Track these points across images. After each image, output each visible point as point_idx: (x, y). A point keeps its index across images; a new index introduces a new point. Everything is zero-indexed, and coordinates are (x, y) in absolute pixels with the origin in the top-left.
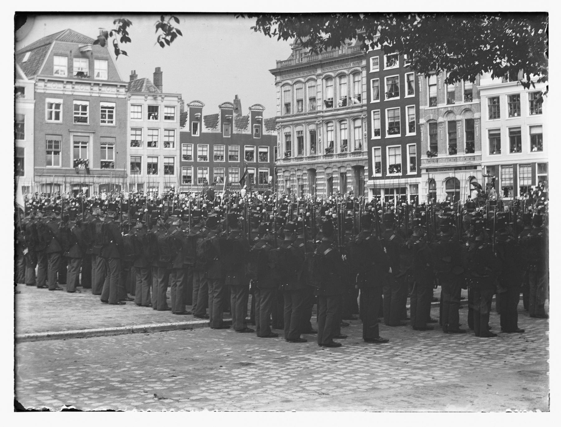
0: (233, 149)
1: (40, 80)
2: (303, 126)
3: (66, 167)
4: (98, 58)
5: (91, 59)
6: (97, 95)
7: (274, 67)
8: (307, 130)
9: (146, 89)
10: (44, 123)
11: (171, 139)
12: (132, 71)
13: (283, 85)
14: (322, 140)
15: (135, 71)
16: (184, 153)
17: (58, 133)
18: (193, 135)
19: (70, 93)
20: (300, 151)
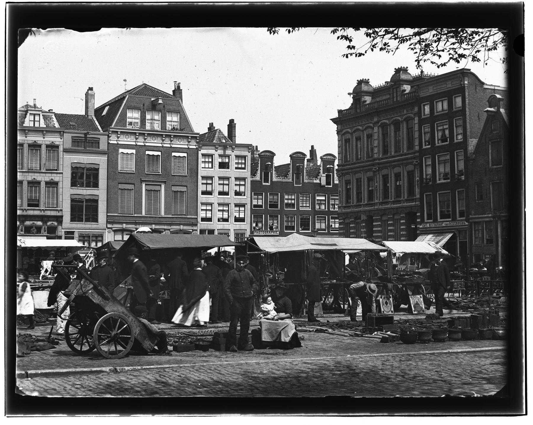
1: (113, 132)
4: (171, 112)
5: (163, 111)
6: (169, 146)
7: (336, 115)
8: (365, 177)
9: (218, 140)
11: (242, 189)
12: (210, 123)
13: (344, 134)
14: (378, 187)
15: (212, 123)
16: (255, 202)
17: (130, 181)
18: (264, 184)
19: (143, 144)
20: (359, 199)
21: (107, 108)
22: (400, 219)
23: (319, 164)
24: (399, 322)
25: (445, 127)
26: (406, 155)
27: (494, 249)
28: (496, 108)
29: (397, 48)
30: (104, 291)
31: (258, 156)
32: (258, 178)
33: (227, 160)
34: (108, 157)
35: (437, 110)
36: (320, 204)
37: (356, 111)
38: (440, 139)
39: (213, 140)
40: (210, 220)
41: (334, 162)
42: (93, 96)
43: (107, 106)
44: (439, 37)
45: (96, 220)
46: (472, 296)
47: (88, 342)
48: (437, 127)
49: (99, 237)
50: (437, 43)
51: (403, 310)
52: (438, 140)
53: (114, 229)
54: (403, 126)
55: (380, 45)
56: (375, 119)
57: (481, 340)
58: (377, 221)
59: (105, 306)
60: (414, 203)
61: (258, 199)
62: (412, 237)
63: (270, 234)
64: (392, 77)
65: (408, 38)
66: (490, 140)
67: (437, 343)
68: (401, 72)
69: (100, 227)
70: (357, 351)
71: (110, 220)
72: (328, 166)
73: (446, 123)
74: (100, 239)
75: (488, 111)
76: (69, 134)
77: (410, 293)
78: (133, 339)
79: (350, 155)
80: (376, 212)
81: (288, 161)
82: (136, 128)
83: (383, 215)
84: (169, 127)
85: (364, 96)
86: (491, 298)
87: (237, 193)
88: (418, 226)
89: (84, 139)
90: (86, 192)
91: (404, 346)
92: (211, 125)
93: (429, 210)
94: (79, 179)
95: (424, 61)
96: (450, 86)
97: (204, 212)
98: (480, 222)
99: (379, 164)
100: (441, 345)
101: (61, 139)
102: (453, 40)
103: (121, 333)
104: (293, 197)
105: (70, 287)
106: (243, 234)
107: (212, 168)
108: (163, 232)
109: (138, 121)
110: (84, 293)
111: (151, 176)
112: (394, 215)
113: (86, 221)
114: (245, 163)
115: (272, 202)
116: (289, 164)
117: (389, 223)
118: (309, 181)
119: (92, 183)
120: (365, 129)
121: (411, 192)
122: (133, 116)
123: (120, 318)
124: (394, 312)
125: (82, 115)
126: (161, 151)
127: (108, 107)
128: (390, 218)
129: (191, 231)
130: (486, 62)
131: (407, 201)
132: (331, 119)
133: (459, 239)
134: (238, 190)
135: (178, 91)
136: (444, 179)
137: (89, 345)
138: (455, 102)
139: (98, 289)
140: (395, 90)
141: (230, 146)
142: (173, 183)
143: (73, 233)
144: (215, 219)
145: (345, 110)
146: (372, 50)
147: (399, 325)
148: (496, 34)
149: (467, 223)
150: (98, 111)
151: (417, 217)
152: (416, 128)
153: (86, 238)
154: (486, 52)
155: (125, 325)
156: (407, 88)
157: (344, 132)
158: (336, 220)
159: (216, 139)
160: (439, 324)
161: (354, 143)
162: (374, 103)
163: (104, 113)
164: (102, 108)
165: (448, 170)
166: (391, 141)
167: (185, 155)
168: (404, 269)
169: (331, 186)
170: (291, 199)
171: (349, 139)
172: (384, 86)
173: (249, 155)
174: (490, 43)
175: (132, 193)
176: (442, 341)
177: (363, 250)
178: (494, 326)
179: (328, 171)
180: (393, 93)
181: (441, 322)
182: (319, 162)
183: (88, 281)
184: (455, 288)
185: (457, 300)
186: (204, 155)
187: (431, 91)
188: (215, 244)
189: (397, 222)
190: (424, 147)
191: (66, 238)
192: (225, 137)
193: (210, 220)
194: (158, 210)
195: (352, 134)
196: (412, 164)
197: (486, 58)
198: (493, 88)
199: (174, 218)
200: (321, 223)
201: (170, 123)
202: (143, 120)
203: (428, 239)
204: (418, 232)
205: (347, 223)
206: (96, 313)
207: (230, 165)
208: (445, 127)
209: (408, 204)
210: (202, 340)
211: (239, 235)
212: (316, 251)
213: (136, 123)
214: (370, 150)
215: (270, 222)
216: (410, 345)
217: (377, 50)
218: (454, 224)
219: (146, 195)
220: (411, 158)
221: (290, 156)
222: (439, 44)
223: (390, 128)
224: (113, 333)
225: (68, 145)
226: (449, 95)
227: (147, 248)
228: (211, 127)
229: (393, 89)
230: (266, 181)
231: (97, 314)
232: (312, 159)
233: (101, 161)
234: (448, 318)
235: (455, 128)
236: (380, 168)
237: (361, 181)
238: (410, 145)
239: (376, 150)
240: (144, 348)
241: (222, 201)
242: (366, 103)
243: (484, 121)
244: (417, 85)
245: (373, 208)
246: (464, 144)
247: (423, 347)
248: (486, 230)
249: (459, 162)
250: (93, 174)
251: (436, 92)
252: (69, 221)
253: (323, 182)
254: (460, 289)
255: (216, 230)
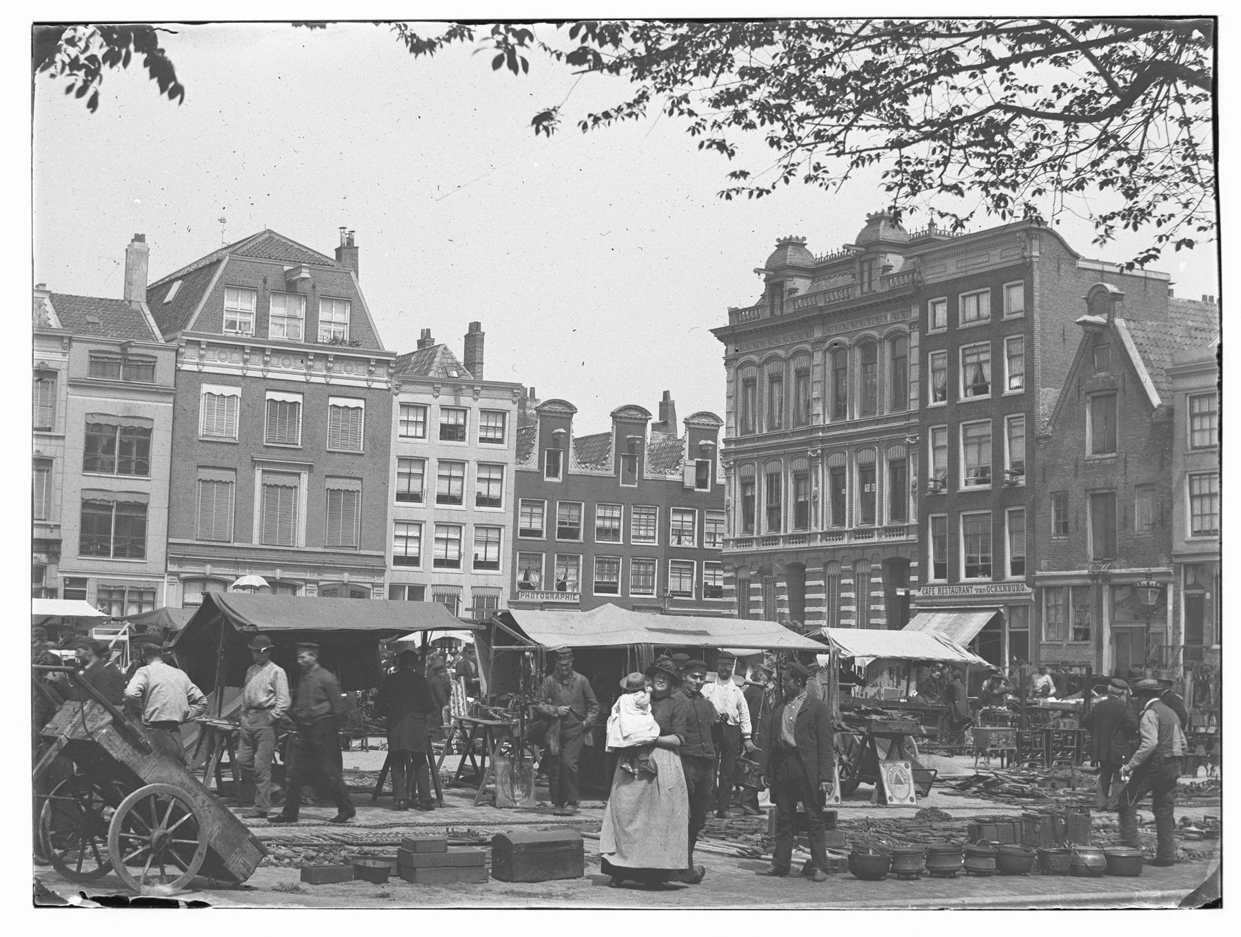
0: (607, 515)
1: (188, 342)
2: (754, 465)
3: (241, 541)
4: (328, 298)
7: (724, 321)
9: (440, 371)
10: (194, 439)
11: (494, 490)
12: (423, 331)
13: (741, 366)
15: (428, 330)
16: (524, 523)
17: (226, 463)
18: (547, 479)
21: (176, 286)
22: (871, 575)
23: (680, 436)
24: (850, 825)
25: (983, 357)
26: (888, 420)
27: (1091, 652)
28: (1106, 315)
29: (846, 178)
30: (138, 730)
31: (535, 412)
32: (532, 464)
33: (461, 421)
34: (174, 403)
35: (935, 324)
36: (679, 534)
37: (772, 312)
38: (969, 387)
39: (428, 370)
40: (414, 561)
41: (717, 431)
42: (144, 255)
43: (177, 279)
44: (946, 153)
45: (139, 552)
46: (1032, 766)
47: (96, 853)
48: (964, 356)
49: (145, 594)
50: (942, 168)
51: (866, 795)
52: (965, 389)
53: (183, 576)
54: (883, 353)
55: (804, 170)
56: (818, 334)
57: (1043, 874)
58: (814, 576)
59: (139, 767)
60: (903, 538)
61: (531, 515)
62: (899, 618)
63: (557, 600)
64: (860, 235)
65: (873, 153)
66: (1088, 393)
67: (937, 880)
68: (883, 223)
69: (149, 570)
70: (742, 895)
71: (175, 556)
72: (702, 442)
73: (984, 349)
74: (149, 598)
75: (1084, 323)
76: (85, 345)
77: (882, 755)
78: (202, 849)
79: (754, 416)
80: (812, 555)
81: (607, 426)
82: (245, 336)
83: (830, 562)
84: (323, 335)
85: (793, 277)
86: (1078, 774)
87: (482, 501)
88: (912, 592)
89: (120, 357)
90: (117, 485)
91: (858, 884)
92: (426, 334)
93: (939, 553)
94: (103, 452)
95: (911, 212)
96: (997, 260)
97: (402, 543)
98: (1061, 587)
99: (823, 440)
100: (946, 884)
101: (64, 354)
102: (981, 164)
103: (175, 834)
104: (616, 514)
105: (56, 718)
106: (493, 599)
107: (424, 437)
108: (301, 587)
109: (252, 319)
110: (90, 734)
111: (277, 451)
112: (855, 563)
113: (115, 555)
114: (503, 429)
115: (566, 523)
116: (608, 435)
117: (843, 581)
118: (657, 475)
119: (133, 464)
120: (793, 357)
121: (898, 510)
122: (239, 306)
123: (174, 797)
124: (842, 800)
125: (117, 301)
126: (303, 394)
127: (180, 282)
128: (848, 571)
129: (369, 586)
130: (1056, 218)
131: (889, 531)
132: (712, 331)
133: (1010, 627)
134: (485, 493)
135: (347, 250)
136: (978, 482)
137: (99, 861)
138: (1009, 300)
139: (124, 727)
140: (866, 267)
141: (468, 387)
142: (329, 470)
143: (83, 582)
144: (427, 562)
145: (745, 310)
146: (787, 181)
147: (851, 832)
148: (1081, 150)
149: (1029, 590)
150: (155, 292)
151: (910, 571)
152: (914, 357)
153: (115, 597)
154: (1058, 193)
155: (186, 814)
156: (896, 262)
157: (742, 360)
158: (717, 573)
159: (434, 368)
160: (947, 833)
161: (766, 390)
162: (815, 295)
163: (170, 297)
164: (166, 284)
165: (987, 460)
166: (852, 386)
167: (361, 404)
168: (872, 697)
169: (708, 490)
170: (612, 518)
171: (754, 380)
172: (842, 256)
173: (513, 410)
174: (1067, 175)
175: (231, 490)
176: (950, 874)
177: (771, 650)
178: (1077, 841)
179: (703, 456)
180: (862, 273)
181: (951, 829)
182: (681, 431)
183: (100, 706)
184: (993, 746)
185: (996, 775)
186: (403, 405)
187: (951, 269)
188: (415, 624)
189: (863, 582)
190: (932, 403)
191: (68, 596)
192: (458, 364)
193: (414, 561)
194: (288, 533)
195: (760, 366)
196: (903, 445)
197: (1058, 209)
198: (1099, 267)
199: (328, 553)
200: (681, 577)
201: (326, 327)
202: (262, 318)
203: (936, 625)
204: (912, 606)
205: (743, 581)
206: (116, 785)
207: (467, 431)
208: (983, 357)
209: (888, 539)
210: (374, 857)
211: (483, 601)
212: (659, 649)
213: (245, 323)
214: (802, 407)
215: (559, 572)
216: (873, 884)
217: (797, 180)
218: (999, 590)
219: (263, 496)
220: (900, 430)
221: (613, 415)
222: (945, 170)
223: (852, 355)
224: (156, 834)
225: (81, 369)
226: (995, 282)
227: (251, 629)
228: (425, 341)
229: (862, 263)
230: (553, 472)
231: (120, 785)
232: (665, 424)
233: (157, 412)
234: (969, 818)
235: (961, 368)
236: (826, 452)
237: (778, 481)
238: (900, 399)
239: (818, 408)
240: (230, 873)
241: (445, 519)
242: (797, 294)
243: (1077, 347)
244: (919, 256)
245: (806, 545)
246: (1024, 402)
247: (903, 889)
248: (1074, 606)
249: (1013, 441)
250: (138, 442)
251: (964, 274)
252: (77, 551)
253: (690, 480)
254: (1004, 747)
255: (429, 587)
